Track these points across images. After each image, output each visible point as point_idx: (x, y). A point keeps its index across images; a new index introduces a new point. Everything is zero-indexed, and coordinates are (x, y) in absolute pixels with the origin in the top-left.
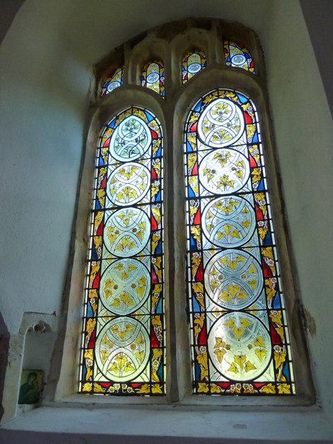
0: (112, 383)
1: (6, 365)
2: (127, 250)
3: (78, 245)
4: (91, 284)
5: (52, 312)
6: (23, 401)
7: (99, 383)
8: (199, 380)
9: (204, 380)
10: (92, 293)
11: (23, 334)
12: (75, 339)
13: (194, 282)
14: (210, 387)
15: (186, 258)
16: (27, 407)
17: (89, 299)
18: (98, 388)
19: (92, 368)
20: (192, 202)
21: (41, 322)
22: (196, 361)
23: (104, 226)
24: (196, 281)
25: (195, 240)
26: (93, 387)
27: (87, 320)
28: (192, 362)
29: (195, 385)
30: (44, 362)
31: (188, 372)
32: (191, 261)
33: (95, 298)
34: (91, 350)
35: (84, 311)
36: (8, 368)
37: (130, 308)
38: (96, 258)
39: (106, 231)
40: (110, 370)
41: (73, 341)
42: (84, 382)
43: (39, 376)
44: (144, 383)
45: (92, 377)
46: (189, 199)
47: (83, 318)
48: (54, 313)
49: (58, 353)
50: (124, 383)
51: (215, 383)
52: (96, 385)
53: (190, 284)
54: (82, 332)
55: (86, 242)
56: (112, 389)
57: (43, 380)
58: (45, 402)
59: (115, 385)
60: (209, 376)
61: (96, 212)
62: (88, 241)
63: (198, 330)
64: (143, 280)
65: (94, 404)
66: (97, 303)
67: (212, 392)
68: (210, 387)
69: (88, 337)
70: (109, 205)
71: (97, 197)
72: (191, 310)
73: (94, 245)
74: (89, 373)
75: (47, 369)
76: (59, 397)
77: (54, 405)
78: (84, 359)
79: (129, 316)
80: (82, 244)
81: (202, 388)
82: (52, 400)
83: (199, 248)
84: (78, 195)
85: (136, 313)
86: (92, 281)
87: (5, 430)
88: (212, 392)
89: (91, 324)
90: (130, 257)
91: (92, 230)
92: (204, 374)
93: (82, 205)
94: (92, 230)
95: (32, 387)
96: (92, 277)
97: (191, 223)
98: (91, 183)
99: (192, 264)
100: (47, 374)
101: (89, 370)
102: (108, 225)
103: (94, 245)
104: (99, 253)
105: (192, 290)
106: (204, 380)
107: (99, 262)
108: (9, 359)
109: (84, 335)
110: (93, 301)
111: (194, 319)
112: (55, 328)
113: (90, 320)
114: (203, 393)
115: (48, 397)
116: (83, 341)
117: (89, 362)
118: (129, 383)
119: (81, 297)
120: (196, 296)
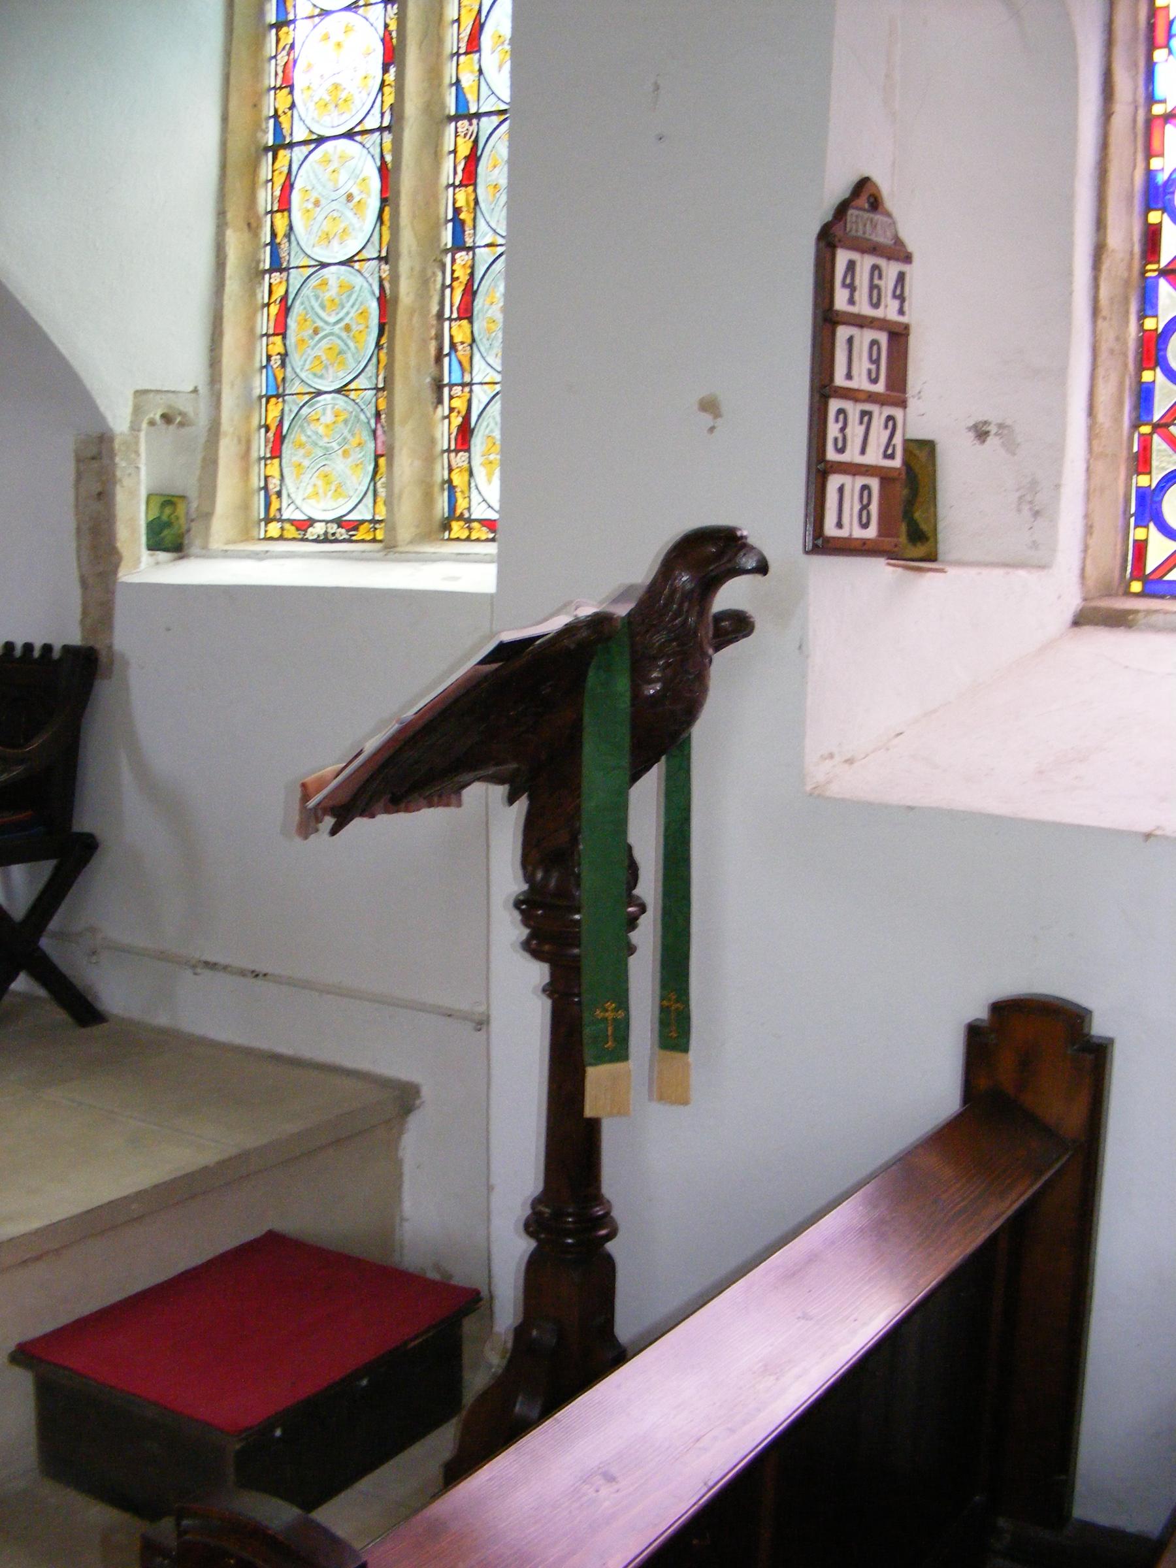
0: (311, 522)
1: (114, 483)
2: (335, 243)
3: (234, 241)
4: (272, 324)
5: (191, 388)
6: (155, 545)
7: (292, 522)
8: (453, 515)
9: (461, 518)
10: (274, 343)
11: (139, 430)
12: (244, 440)
13: (456, 320)
14: (470, 529)
15: (443, 266)
16: (162, 556)
17: (269, 357)
18: (291, 531)
19: (279, 494)
20: (463, 125)
21: (170, 407)
22: (450, 481)
23: (292, 186)
24: (459, 318)
25: (463, 222)
26: (282, 529)
27: (267, 402)
28: (444, 482)
29: (446, 526)
30: (187, 482)
31: (428, 500)
32: (453, 272)
33: (279, 354)
34: (276, 461)
35: (260, 385)
36: (118, 487)
37: (341, 374)
38: (277, 266)
39: (296, 197)
40: (308, 498)
41: (239, 441)
42: (268, 520)
43: (181, 509)
44: (363, 522)
45: (280, 510)
46: (457, 118)
47: (260, 397)
48: (195, 391)
49: (210, 463)
50: (332, 521)
51: (480, 521)
52: (287, 526)
53: (447, 324)
54: (260, 427)
55: (253, 227)
56: (318, 530)
57: (187, 513)
58: (194, 550)
59: (317, 525)
60: (469, 509)
61: (275, 150)
62: (259, 226)
63: (457, 421)
64: (363, 314)
65: (267, 552)
66: (283, 365)
67: (474, 537)
68: (470, 529)
69: (271, 434)
70: (300, 135)
71: (276, 111)
72: (446, 381)
73: (274, 235)
74: (275, 505)
75: (193, 494)
76: (216, 543)
77: (207, 554)
78: (266, 478)
79: (338, 391)
80: (246, 236)
81: (457, 529)
82: (205, 547)
83: (469, 243)
84: (225, 119)
85: (352, 386)
86: (272, 318)
87: (126, 583)
88: (474, 537)
89: (274, 412)
90: (341, 263)
91: (265, 198)
92: (461, 504)
93: (238, 144)
94: (265, 198)
95: (169, 524)
96: (274, 309)
97: (457, 183)
98: (257, 73)
99: (453, 279)
100: (194, 505)
101: (274, 498)
102: (298, 185)
103: (274, 235)
104: (283, 254)
105: (451, 337)
106: (461, 518)
107: (285, 274)
108: (119, 474)
109: (263, 430)
110: (276, 361)
111: (451, 398)
112: (202, 421)
113: (273, 400)
114: (458, 539)
115: (198, 542)
116: (260, 446)
117: (274, 485)
118: (339, 522)
119: (250, 353)
120: (456, 351)
